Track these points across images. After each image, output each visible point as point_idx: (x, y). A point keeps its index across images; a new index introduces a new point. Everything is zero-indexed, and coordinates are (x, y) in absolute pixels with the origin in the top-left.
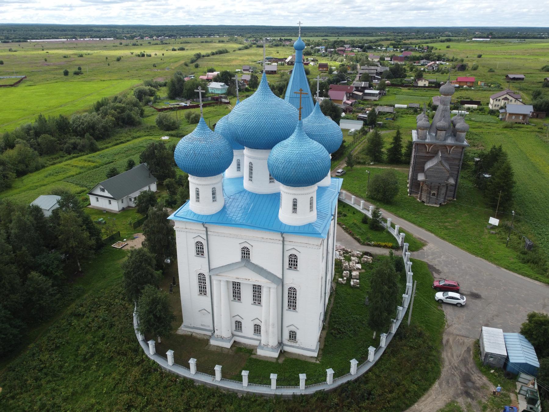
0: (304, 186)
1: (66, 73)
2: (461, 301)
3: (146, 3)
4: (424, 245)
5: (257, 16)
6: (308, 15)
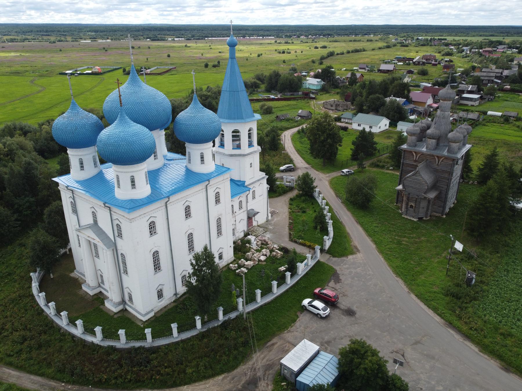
0: (129, 165)
1: (206, 66)
2: (321, 312)
4: (352, 253)
5: (426, 15)
6: (482, 13)
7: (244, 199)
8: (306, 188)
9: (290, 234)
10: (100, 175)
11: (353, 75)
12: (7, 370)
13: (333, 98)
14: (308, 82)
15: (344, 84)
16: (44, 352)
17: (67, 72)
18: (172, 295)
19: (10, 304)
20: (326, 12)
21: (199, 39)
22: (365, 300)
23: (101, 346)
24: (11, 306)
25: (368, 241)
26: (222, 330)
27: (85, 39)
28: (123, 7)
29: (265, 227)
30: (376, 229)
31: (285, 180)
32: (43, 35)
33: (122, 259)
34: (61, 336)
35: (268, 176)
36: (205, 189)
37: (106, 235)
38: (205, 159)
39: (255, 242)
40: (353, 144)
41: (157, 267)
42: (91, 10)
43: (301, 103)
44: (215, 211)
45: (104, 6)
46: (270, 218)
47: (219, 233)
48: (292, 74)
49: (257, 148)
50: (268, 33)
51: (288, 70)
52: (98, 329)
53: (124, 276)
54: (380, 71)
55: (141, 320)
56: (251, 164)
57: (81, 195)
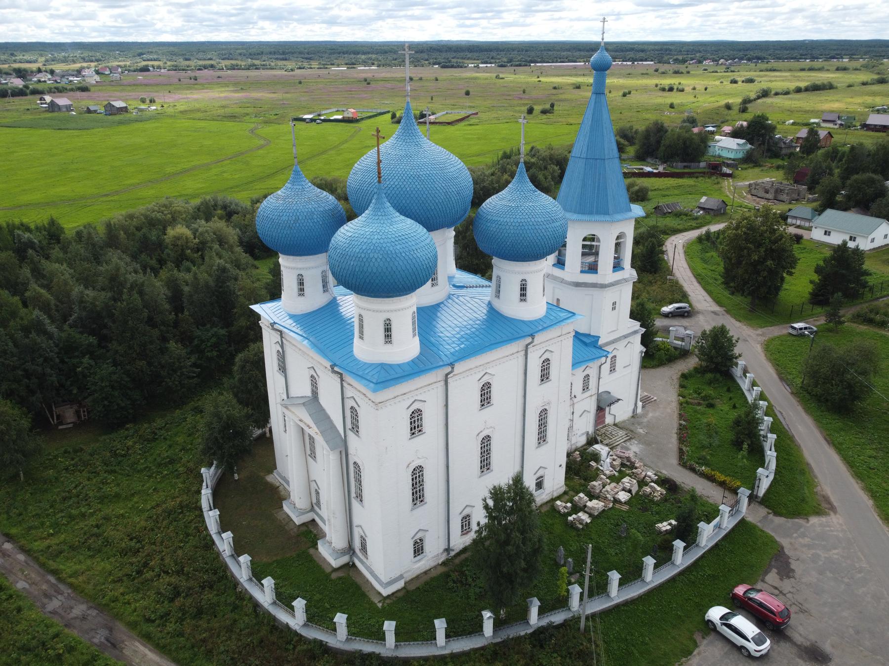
0: (383, 297)
1: (530, 111)
2: (751, 646)
3: (737, 4)
4: (818, 512)
7: (593, 372)
8: (717, 357)
9: (681, 450)
10: (332, 306)
11: (813, 133)
12: (142, 648)
13: (770, 177)
14: (718, 144)
15: (792, 150)
16: (205, 625)
17: (305, 117)
18: (441, 551)
19: (163, 520)
20: (756, 17)
21: (520, 65)
22: (851, 631)
23: (301, 636)
24: (165, 523)
25: (855, 488)
26: (534, 646)
27: (338, 66)
28: (402, 13)
29: (628, 428)
30: (874, 463)
31: (672, 335)
32: (277, 59)
33: (355, 473)
34: (237, 598)
35: (644, 330)
36: (523, 353)
37: (331, 422)
38: (529, 292)
39: (608, 460)
40: (816, 272)
41: (418, 496)
42: (351, 19)
43: (704, 183)
44: (538, 395)
45: (371, 13)
46: (639, 410)
47: (542, 437)
48: (688, 130)
49: (629, 273)
50: (642, 55)
51: (679, 121)
52: (299, 604)
53: (355, 504)
54: (866, 127)
55: (379, 593)
56: (614, 304)
57: (294, 342)
